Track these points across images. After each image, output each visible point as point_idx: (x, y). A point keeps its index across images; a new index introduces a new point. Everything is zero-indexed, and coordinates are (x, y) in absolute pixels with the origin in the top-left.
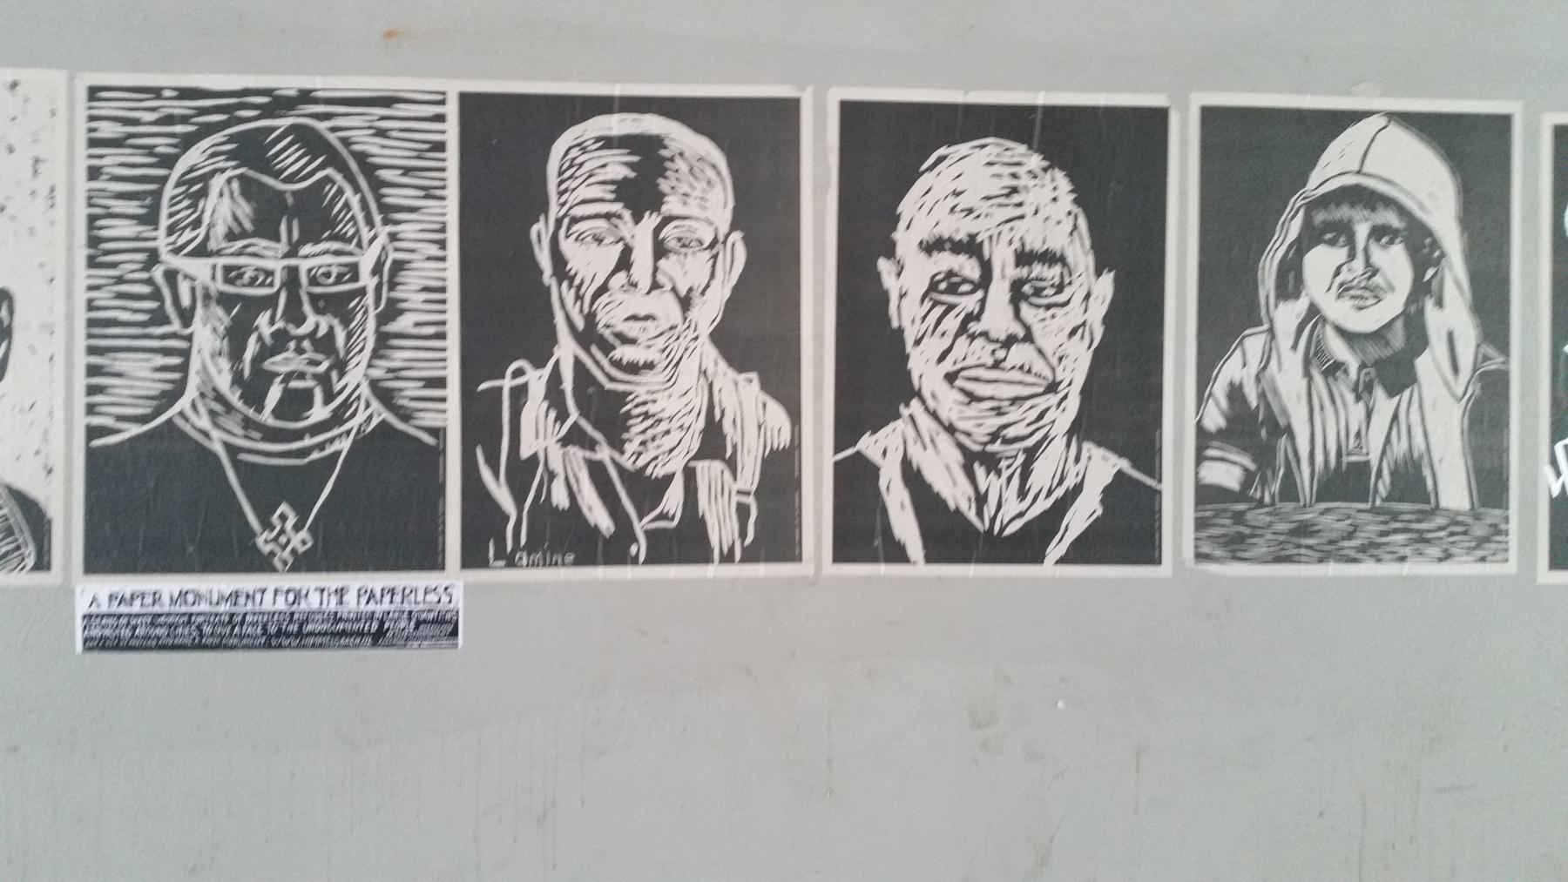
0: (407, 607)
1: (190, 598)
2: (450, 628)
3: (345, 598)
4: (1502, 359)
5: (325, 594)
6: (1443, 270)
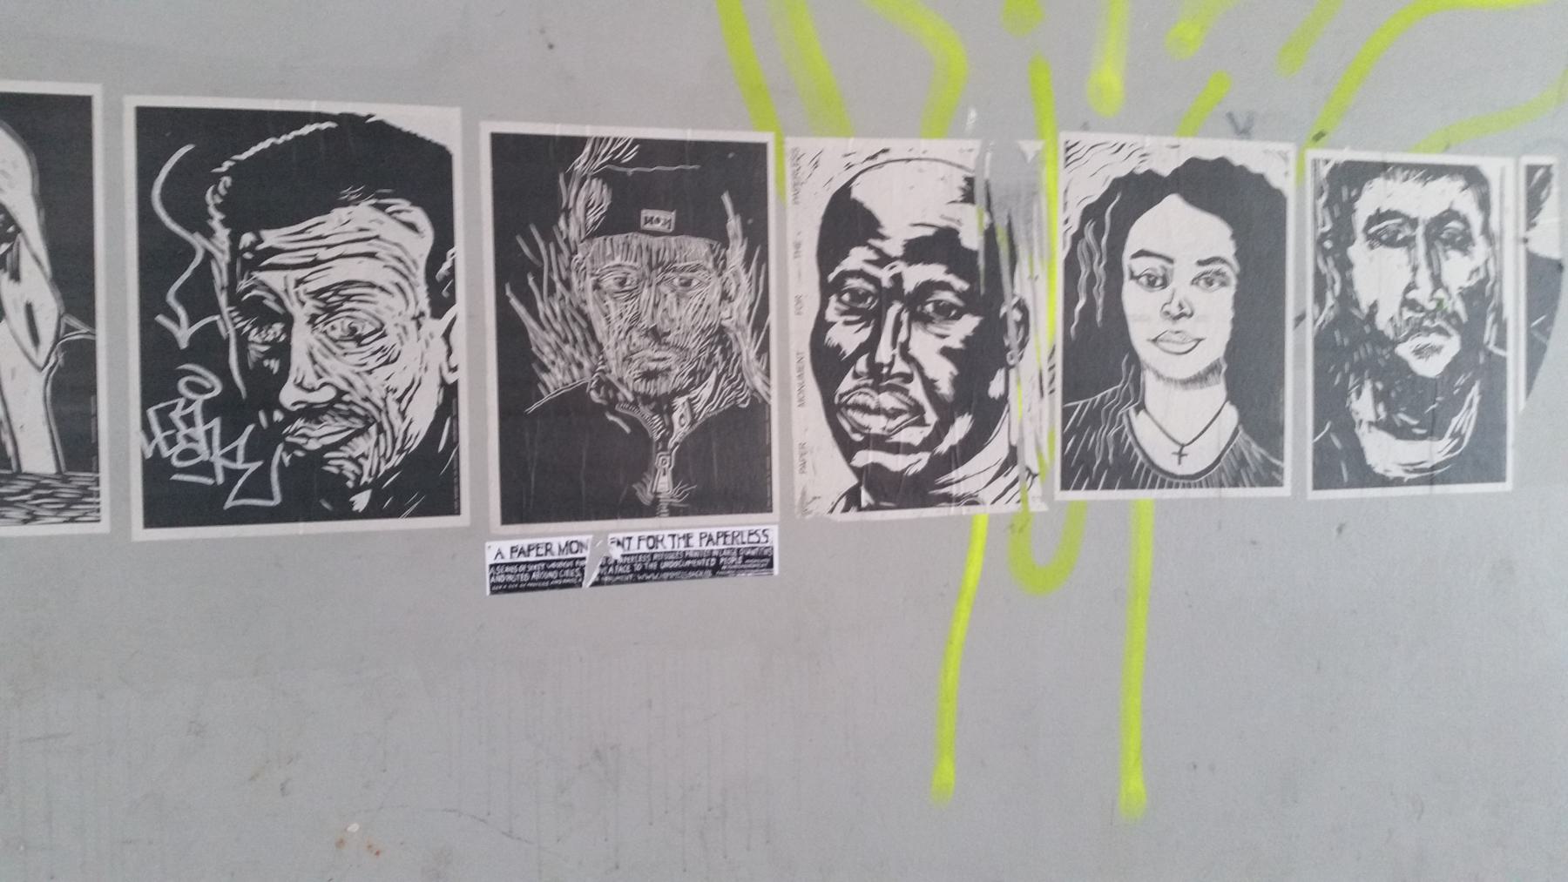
0: (736, 546)
1: (575, 547)
2: (768, 560)
3: (691, 541)
4: (85, 330)
5: (676, 538)
6: (18, 245)
